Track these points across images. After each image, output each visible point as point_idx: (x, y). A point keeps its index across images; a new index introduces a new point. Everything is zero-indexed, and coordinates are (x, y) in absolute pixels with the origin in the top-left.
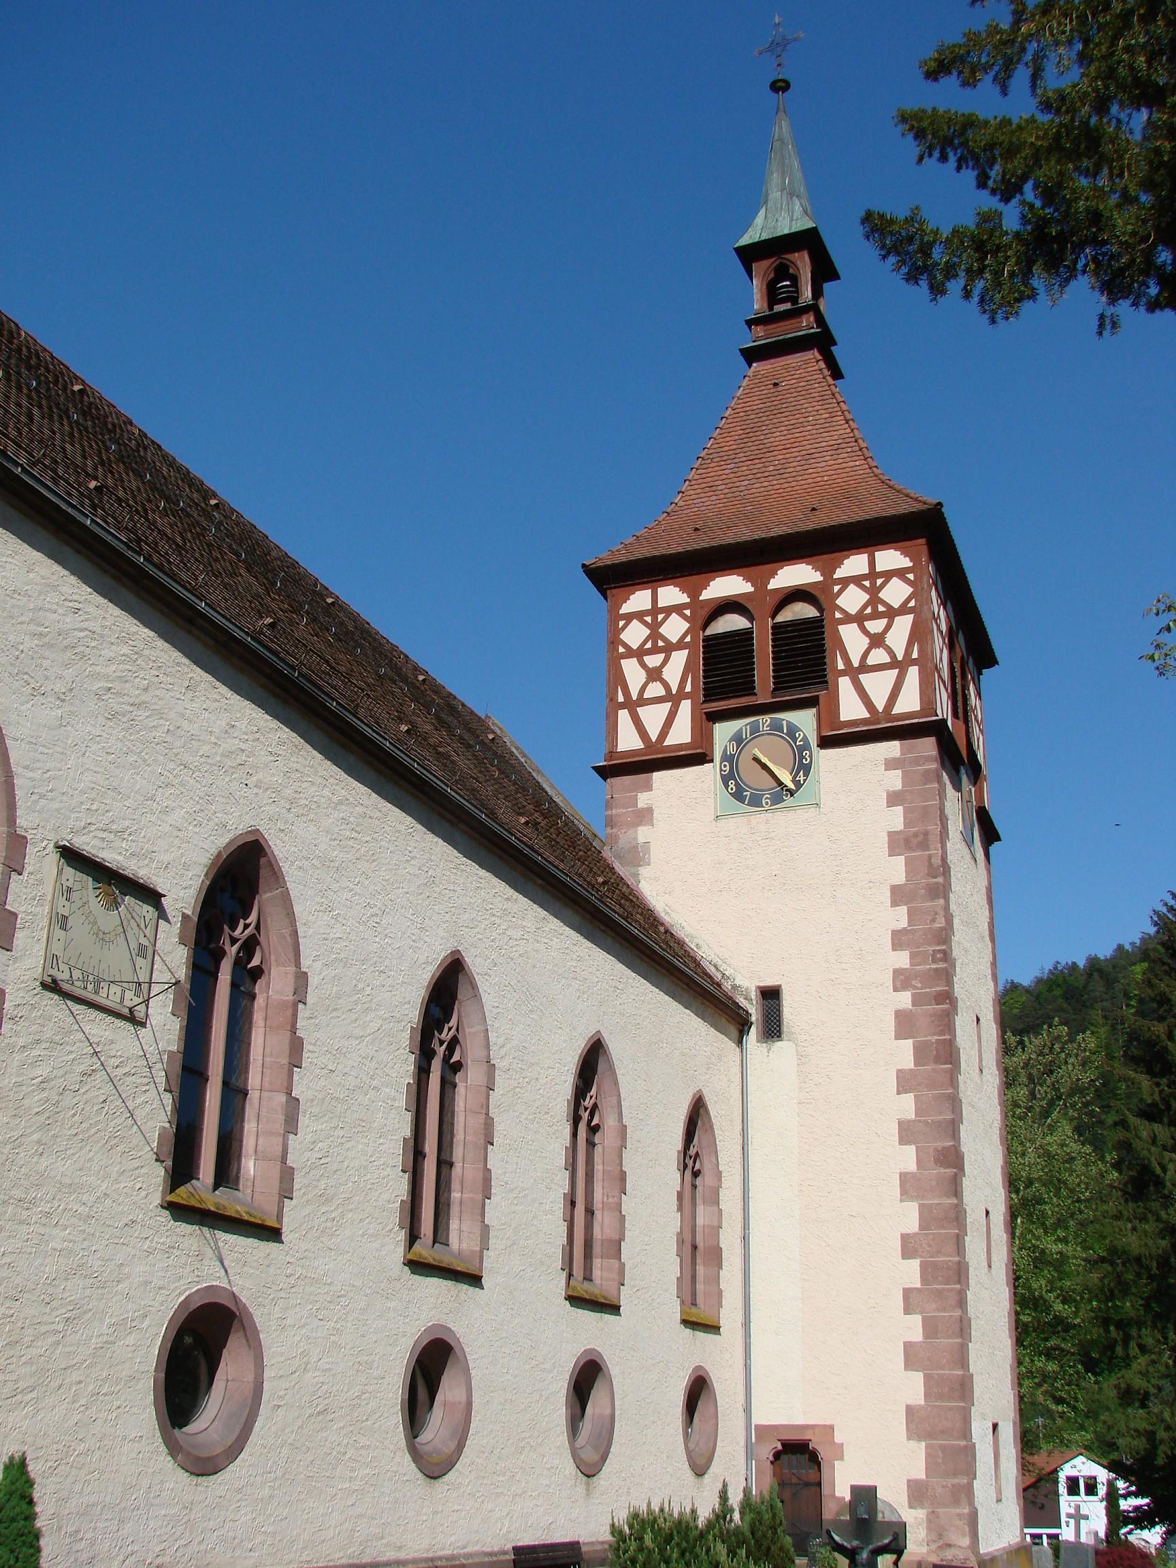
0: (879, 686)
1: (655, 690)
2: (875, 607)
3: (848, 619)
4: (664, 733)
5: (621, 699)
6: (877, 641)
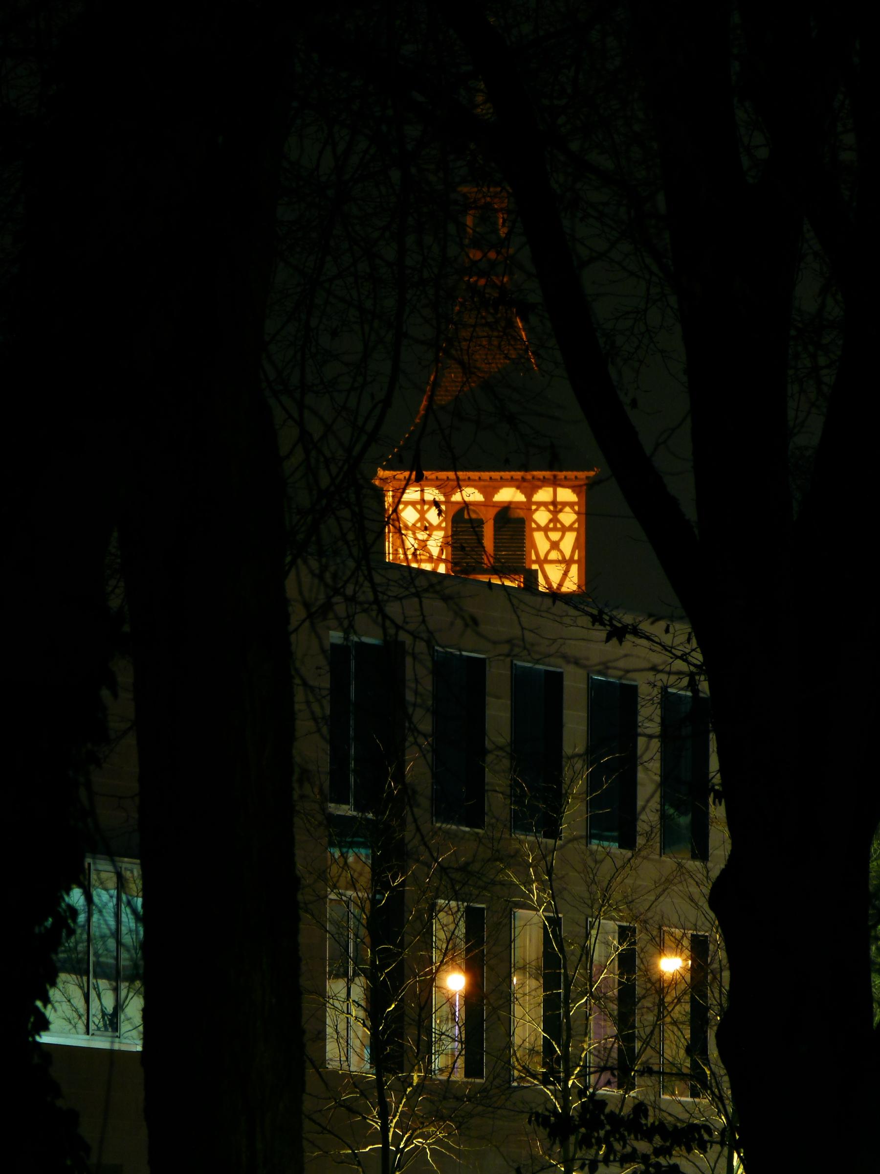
1: (554, 555)
2: (554, 523)
3: (539, 528)
4: (560, 585)
6: (555, 545)
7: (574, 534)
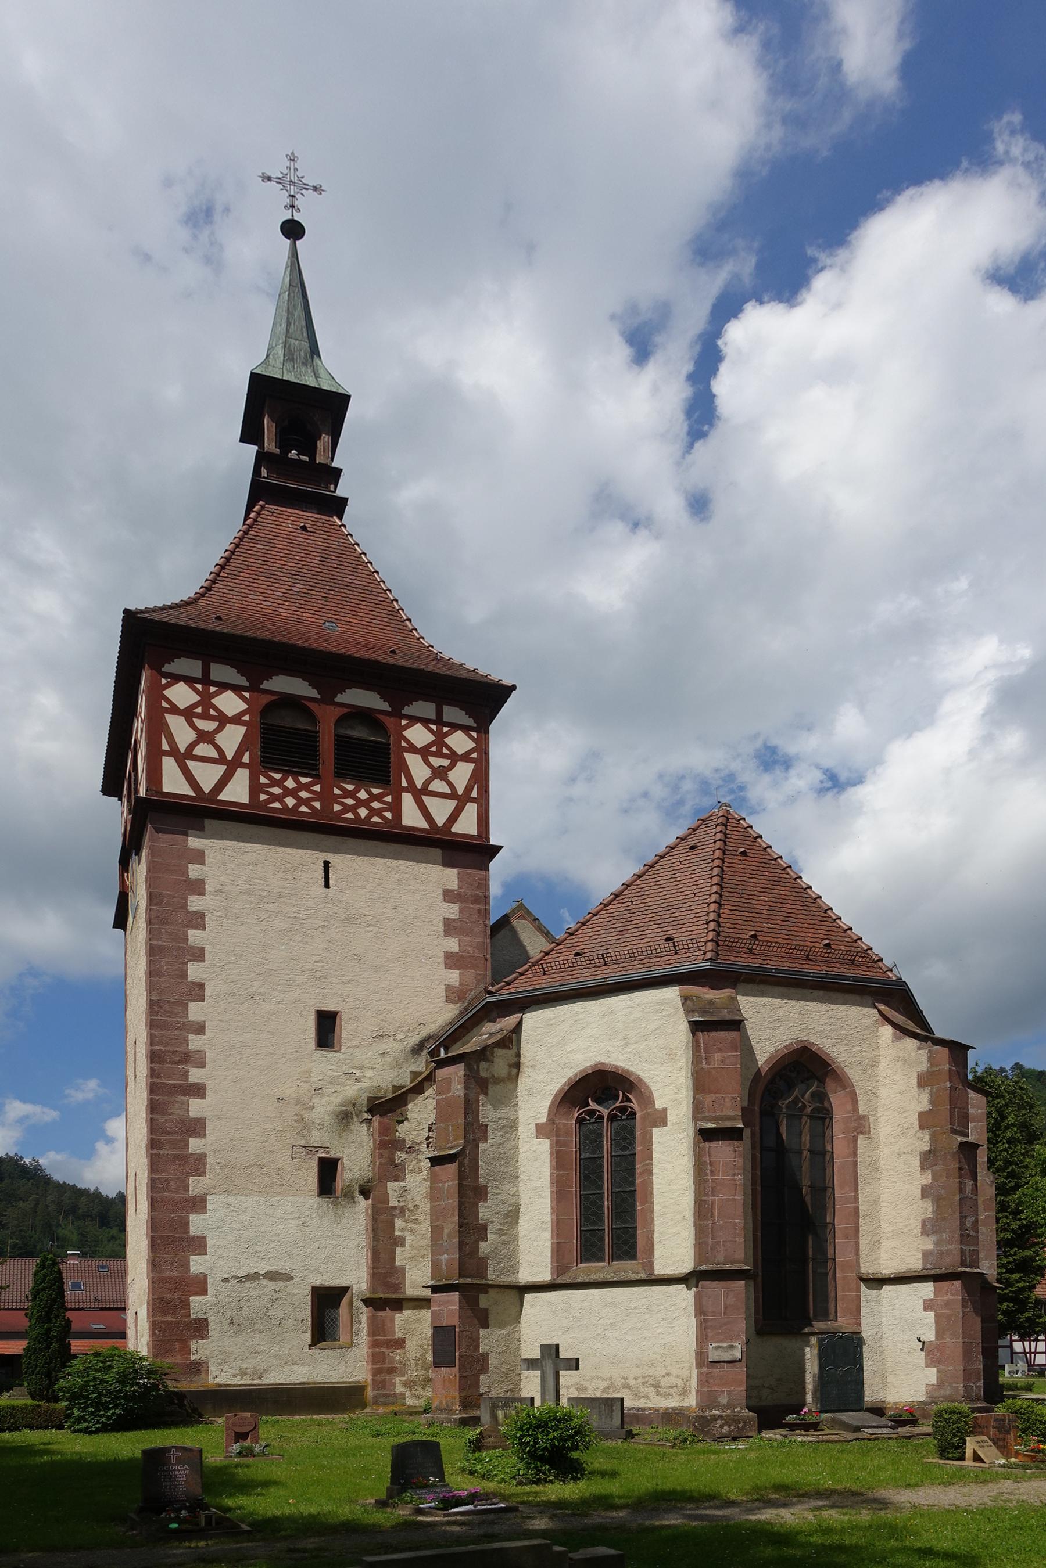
0: (441, 810)
3: (413, 749)
4: (453, 818)
5: (165, 747)
7: (242, 730)
